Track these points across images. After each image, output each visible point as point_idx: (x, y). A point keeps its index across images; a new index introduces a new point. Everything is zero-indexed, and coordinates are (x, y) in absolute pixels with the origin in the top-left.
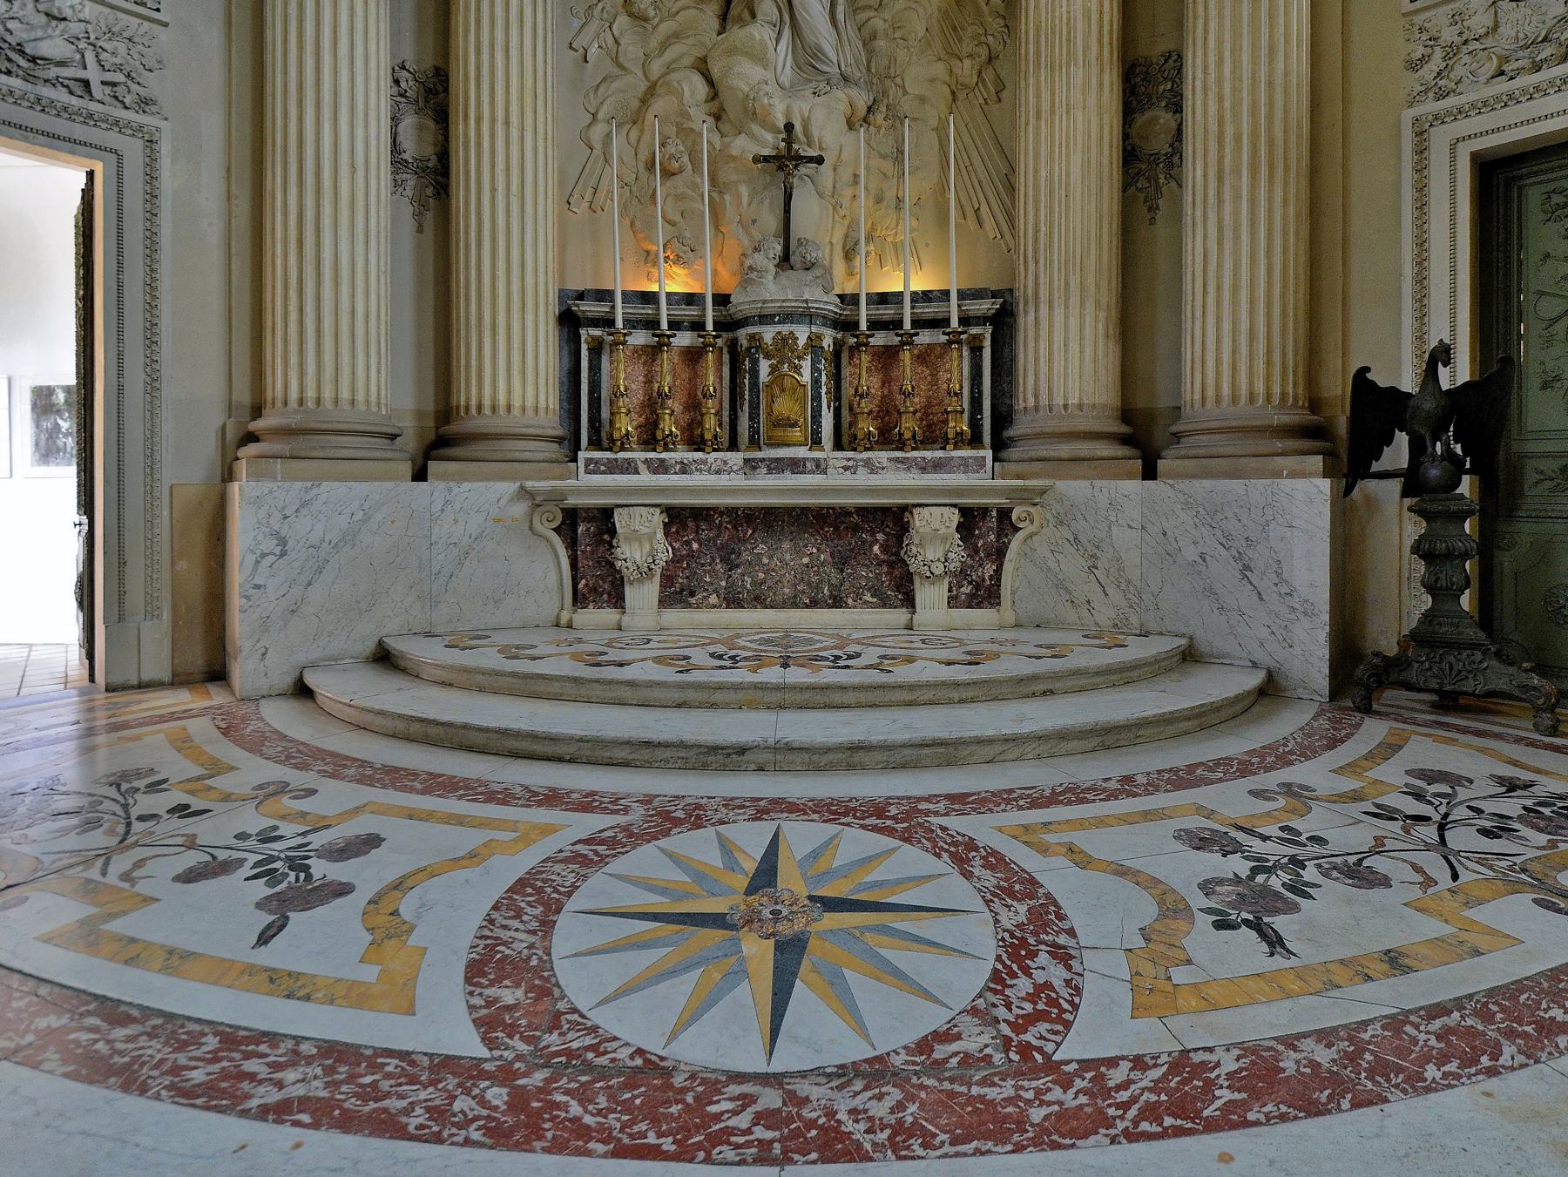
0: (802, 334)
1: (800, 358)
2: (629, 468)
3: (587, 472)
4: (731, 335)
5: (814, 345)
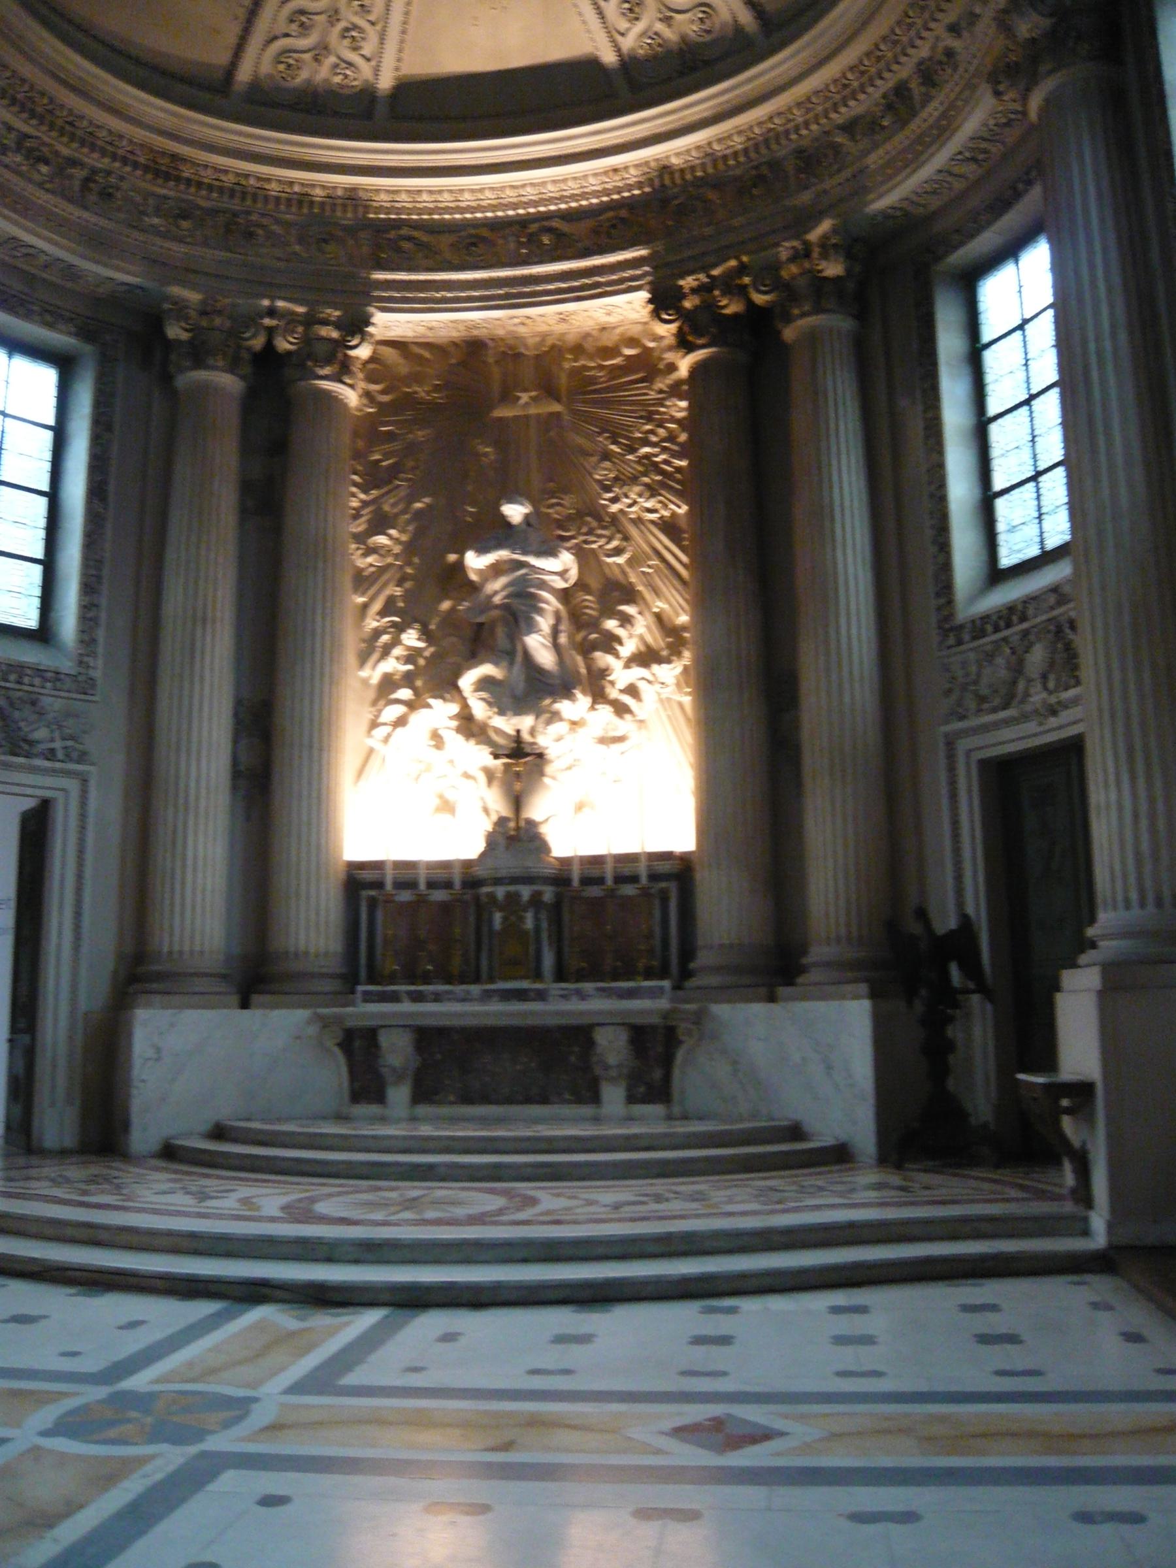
0: (526, 892)
1: (525, 910)
2: (394, 998)
3: (365, 1001)
4: (474, 891)
5: (536, 899)
